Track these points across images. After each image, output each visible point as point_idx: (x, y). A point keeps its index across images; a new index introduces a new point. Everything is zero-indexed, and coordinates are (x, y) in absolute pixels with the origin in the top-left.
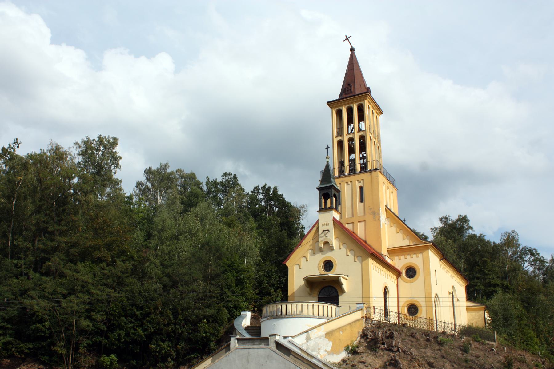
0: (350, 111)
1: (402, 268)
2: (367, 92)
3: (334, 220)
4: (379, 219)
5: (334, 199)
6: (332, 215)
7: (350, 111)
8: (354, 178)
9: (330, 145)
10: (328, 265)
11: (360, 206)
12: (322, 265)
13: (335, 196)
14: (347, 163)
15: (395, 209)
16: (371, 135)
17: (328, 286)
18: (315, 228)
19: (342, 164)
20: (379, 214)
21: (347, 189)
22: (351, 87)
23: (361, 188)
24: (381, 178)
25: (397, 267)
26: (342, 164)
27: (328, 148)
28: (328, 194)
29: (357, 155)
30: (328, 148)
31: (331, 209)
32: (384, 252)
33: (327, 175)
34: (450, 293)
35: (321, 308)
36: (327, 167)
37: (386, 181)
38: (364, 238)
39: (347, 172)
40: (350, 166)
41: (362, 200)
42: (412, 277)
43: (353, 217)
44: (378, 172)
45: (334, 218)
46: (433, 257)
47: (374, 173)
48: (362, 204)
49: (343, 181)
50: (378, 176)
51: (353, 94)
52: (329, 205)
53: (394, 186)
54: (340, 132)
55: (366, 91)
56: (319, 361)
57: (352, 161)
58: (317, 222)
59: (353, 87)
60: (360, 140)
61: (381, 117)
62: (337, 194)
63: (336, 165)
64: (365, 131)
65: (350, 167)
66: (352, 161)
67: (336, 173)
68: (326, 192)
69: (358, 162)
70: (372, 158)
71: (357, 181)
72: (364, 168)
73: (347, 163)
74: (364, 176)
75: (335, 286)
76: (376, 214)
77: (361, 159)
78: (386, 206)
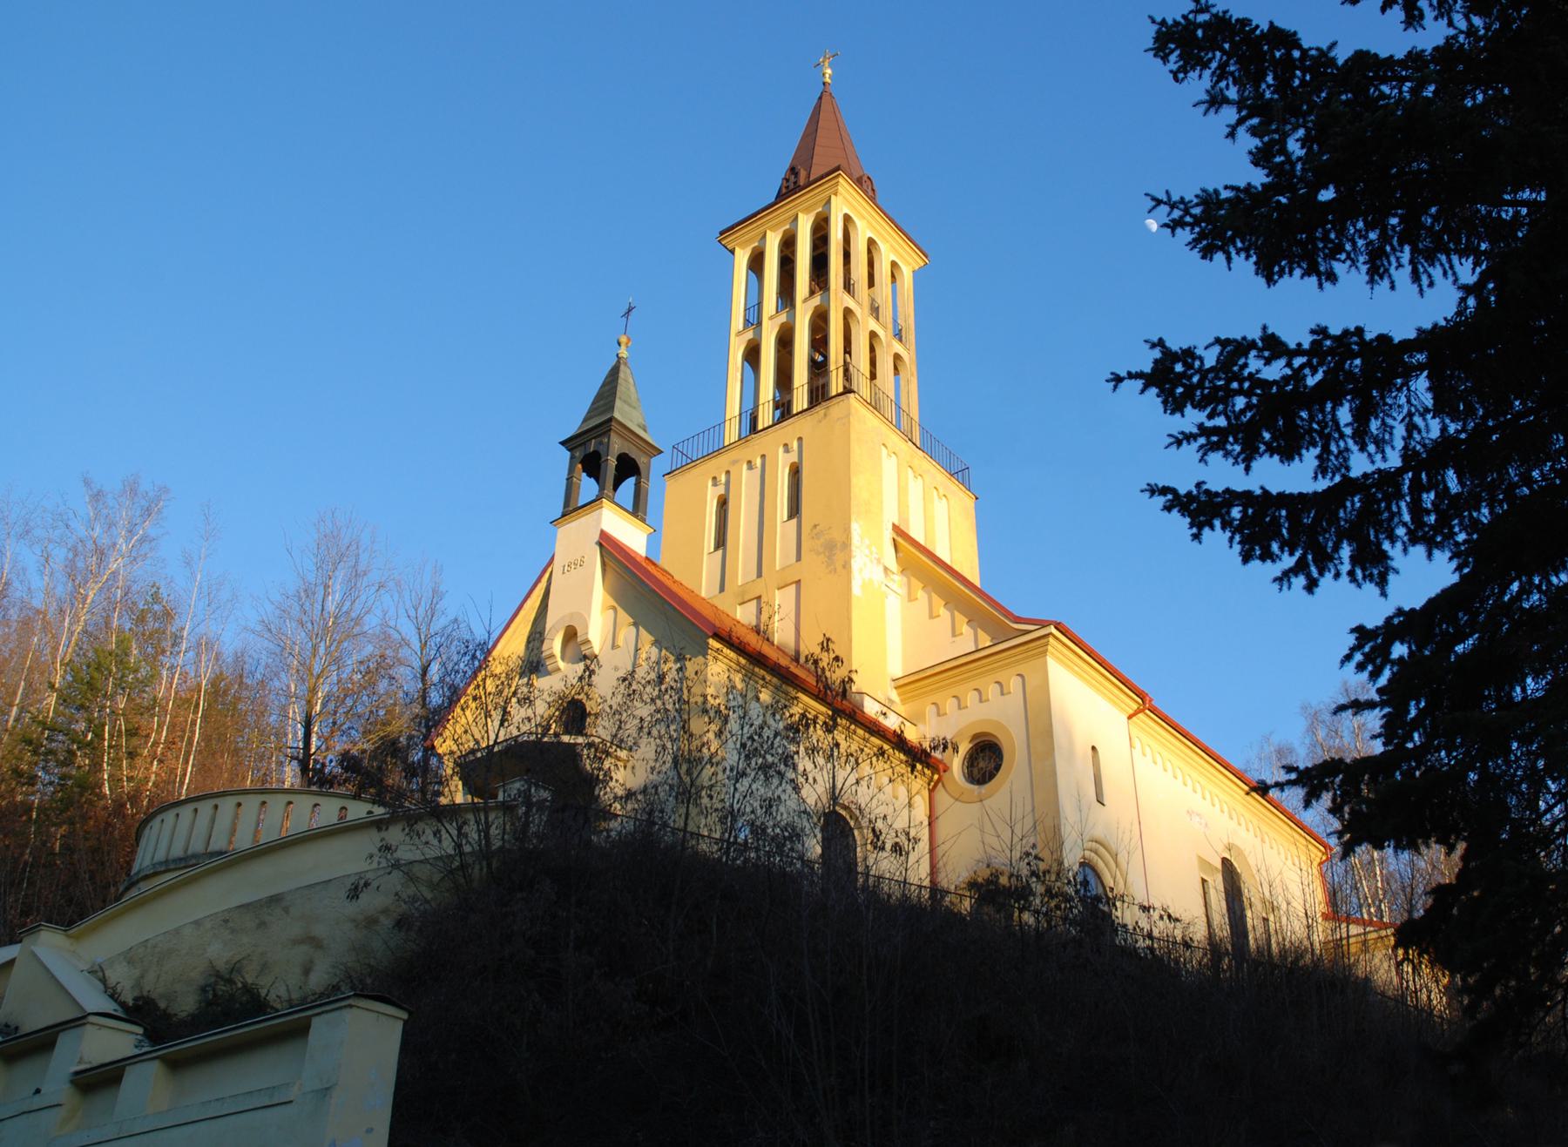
4: (847, 566)
6: (599, 520)
23: (796, 472)
41: (795, 510)
45: (603, 534)
49: (734, 462)
76: (837, 551)
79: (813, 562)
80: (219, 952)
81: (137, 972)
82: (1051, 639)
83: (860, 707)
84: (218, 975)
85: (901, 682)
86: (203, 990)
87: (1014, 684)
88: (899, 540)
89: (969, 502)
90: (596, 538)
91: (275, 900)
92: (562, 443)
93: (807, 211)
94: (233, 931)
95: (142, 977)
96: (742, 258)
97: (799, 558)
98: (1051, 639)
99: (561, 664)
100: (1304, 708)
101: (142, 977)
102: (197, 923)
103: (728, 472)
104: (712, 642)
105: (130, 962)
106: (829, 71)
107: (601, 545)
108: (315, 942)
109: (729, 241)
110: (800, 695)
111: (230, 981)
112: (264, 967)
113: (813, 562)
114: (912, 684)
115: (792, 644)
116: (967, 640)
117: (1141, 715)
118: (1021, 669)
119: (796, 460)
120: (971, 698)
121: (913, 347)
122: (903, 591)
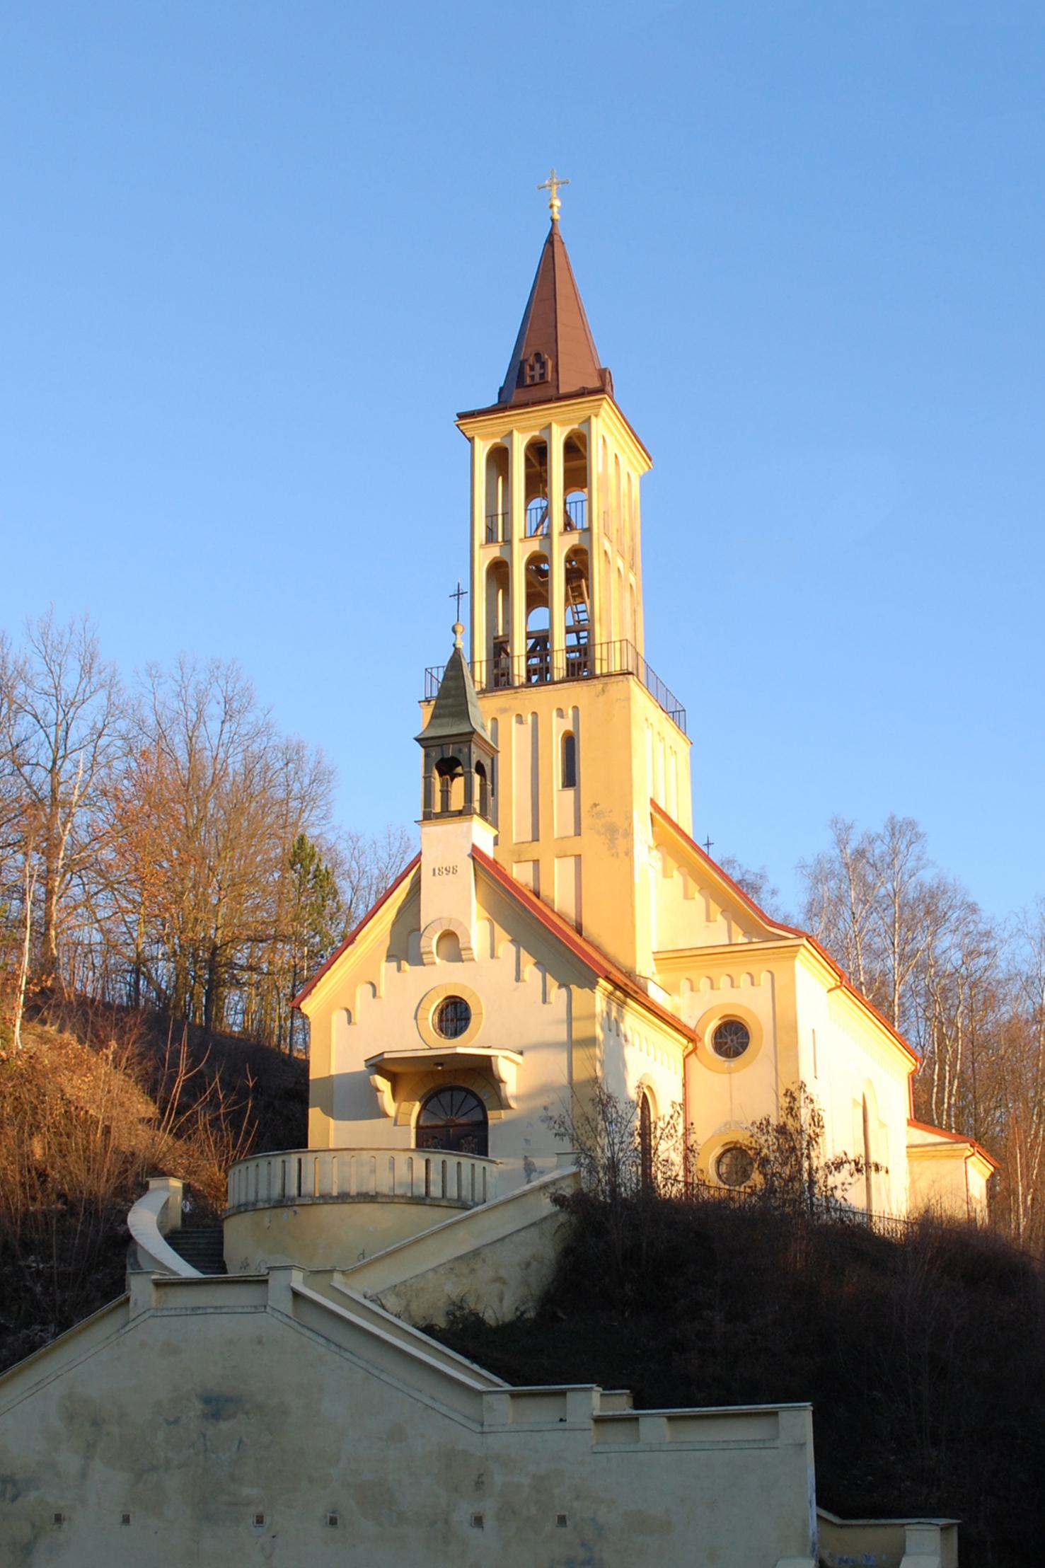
0: (538, 451)
1: (703, 1020)
2: (601, 391)
3: (476, 855)
4: (629, 853)
5: (477, 778)
7: (538, 451)
8: (541, 698)
9: (466, 587)
10: (455, 1015)
11: (559, 800)
12: (430, 1016)
13: (480, 769)
14: (520, 646)
15: (684, 817)
16: (607, 546)
17: (452, 1089)
18: (406, 883)
19: (499, 648)
20: (629, 834)
21: (517, 730)
22: (543, 365)
23: (570, 743)
24: (641, 703)
25: (684, 1018)
26: (499, 648)
27: (459, 594)
28: (453, 757)
29: (559, 614)
30: (459, 594)
31: (464, 813)
32: (644, 966)
33: (451, 696)
34: (855, 1102)
35: (479, 1170)
36: (455, 664)
37: (657, 715)
38: (571, 912)
39: (519, 668)
40: (530, 654)
41: (570, 779)
42: (744, 1046)
43: (536, 838)
44: (630, 677)
45: (474, 848)
46: (810, 977)
47: (615, 687)
48: (570, 793)
49: (503, 711)
50: (628, 699)
51: (552, 392)
52: (457, 802)
53: (681, 726)
54: (497, 530)
55: (596, 384)
56: (219, 1310)
57: (540, 642)
58: (418, 859)
59: (550, 364)
60: (568, 560)
61: (651, 795)
62: (487, 763)
63: (481, 653)
64: (589, 530)
65: (528, 658)
66: (540, 642)
67: (481, 673)
68: (450, 752)
69: (560, 641)
70: (609, 635)
71: (555, 707)
72: (581, 667)
73: (520, 646)
74: (578, 693)
75: (476, 1091)
76: (618, 835)
77: (568, 630)
78: (653, 802)
79: (591, 843)
80: (452, 1289)
81: (404, 1303)
82: (802, 949)
83: (644, 992)
84: (454, 1304)
85: (661, 956)
86: (448, 1314)
87: (764, 978)
88: (658, 817)
89: (683, 748)
90: (469, 851)
91: (476, 1253)
92: (417, 740)
93: (562, 423)
94: (457, 1276)
95: (408, 1305)
96: (482, 450)
97: (578, 832)
98: (802, 949)
99: (437, 960)
100: (834, 822)
101: (408, 1305)
102: (434, 1270)
103: (495, 720)
104: (601, 981)
105: (398, 1295)
106: (557, 203)
107: (474, 859)
108: (500, 1279)
109: (470, 427)
110: (629, 1000)
111: (461, 1308)
112: (478, 1298)
113: (591, 843)
114: (669, 958)
115: (531, 885)
116: (718, 932)
117: (838, 991)
118: (771, 966)
119: (571, 728)
120: (724, 982)
121: (639, 572)
122: (659, 865)
